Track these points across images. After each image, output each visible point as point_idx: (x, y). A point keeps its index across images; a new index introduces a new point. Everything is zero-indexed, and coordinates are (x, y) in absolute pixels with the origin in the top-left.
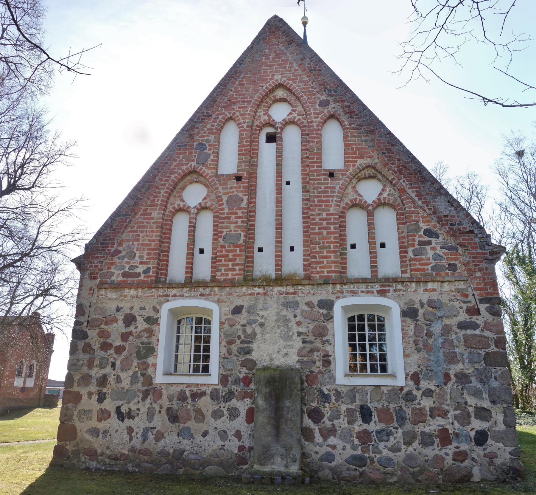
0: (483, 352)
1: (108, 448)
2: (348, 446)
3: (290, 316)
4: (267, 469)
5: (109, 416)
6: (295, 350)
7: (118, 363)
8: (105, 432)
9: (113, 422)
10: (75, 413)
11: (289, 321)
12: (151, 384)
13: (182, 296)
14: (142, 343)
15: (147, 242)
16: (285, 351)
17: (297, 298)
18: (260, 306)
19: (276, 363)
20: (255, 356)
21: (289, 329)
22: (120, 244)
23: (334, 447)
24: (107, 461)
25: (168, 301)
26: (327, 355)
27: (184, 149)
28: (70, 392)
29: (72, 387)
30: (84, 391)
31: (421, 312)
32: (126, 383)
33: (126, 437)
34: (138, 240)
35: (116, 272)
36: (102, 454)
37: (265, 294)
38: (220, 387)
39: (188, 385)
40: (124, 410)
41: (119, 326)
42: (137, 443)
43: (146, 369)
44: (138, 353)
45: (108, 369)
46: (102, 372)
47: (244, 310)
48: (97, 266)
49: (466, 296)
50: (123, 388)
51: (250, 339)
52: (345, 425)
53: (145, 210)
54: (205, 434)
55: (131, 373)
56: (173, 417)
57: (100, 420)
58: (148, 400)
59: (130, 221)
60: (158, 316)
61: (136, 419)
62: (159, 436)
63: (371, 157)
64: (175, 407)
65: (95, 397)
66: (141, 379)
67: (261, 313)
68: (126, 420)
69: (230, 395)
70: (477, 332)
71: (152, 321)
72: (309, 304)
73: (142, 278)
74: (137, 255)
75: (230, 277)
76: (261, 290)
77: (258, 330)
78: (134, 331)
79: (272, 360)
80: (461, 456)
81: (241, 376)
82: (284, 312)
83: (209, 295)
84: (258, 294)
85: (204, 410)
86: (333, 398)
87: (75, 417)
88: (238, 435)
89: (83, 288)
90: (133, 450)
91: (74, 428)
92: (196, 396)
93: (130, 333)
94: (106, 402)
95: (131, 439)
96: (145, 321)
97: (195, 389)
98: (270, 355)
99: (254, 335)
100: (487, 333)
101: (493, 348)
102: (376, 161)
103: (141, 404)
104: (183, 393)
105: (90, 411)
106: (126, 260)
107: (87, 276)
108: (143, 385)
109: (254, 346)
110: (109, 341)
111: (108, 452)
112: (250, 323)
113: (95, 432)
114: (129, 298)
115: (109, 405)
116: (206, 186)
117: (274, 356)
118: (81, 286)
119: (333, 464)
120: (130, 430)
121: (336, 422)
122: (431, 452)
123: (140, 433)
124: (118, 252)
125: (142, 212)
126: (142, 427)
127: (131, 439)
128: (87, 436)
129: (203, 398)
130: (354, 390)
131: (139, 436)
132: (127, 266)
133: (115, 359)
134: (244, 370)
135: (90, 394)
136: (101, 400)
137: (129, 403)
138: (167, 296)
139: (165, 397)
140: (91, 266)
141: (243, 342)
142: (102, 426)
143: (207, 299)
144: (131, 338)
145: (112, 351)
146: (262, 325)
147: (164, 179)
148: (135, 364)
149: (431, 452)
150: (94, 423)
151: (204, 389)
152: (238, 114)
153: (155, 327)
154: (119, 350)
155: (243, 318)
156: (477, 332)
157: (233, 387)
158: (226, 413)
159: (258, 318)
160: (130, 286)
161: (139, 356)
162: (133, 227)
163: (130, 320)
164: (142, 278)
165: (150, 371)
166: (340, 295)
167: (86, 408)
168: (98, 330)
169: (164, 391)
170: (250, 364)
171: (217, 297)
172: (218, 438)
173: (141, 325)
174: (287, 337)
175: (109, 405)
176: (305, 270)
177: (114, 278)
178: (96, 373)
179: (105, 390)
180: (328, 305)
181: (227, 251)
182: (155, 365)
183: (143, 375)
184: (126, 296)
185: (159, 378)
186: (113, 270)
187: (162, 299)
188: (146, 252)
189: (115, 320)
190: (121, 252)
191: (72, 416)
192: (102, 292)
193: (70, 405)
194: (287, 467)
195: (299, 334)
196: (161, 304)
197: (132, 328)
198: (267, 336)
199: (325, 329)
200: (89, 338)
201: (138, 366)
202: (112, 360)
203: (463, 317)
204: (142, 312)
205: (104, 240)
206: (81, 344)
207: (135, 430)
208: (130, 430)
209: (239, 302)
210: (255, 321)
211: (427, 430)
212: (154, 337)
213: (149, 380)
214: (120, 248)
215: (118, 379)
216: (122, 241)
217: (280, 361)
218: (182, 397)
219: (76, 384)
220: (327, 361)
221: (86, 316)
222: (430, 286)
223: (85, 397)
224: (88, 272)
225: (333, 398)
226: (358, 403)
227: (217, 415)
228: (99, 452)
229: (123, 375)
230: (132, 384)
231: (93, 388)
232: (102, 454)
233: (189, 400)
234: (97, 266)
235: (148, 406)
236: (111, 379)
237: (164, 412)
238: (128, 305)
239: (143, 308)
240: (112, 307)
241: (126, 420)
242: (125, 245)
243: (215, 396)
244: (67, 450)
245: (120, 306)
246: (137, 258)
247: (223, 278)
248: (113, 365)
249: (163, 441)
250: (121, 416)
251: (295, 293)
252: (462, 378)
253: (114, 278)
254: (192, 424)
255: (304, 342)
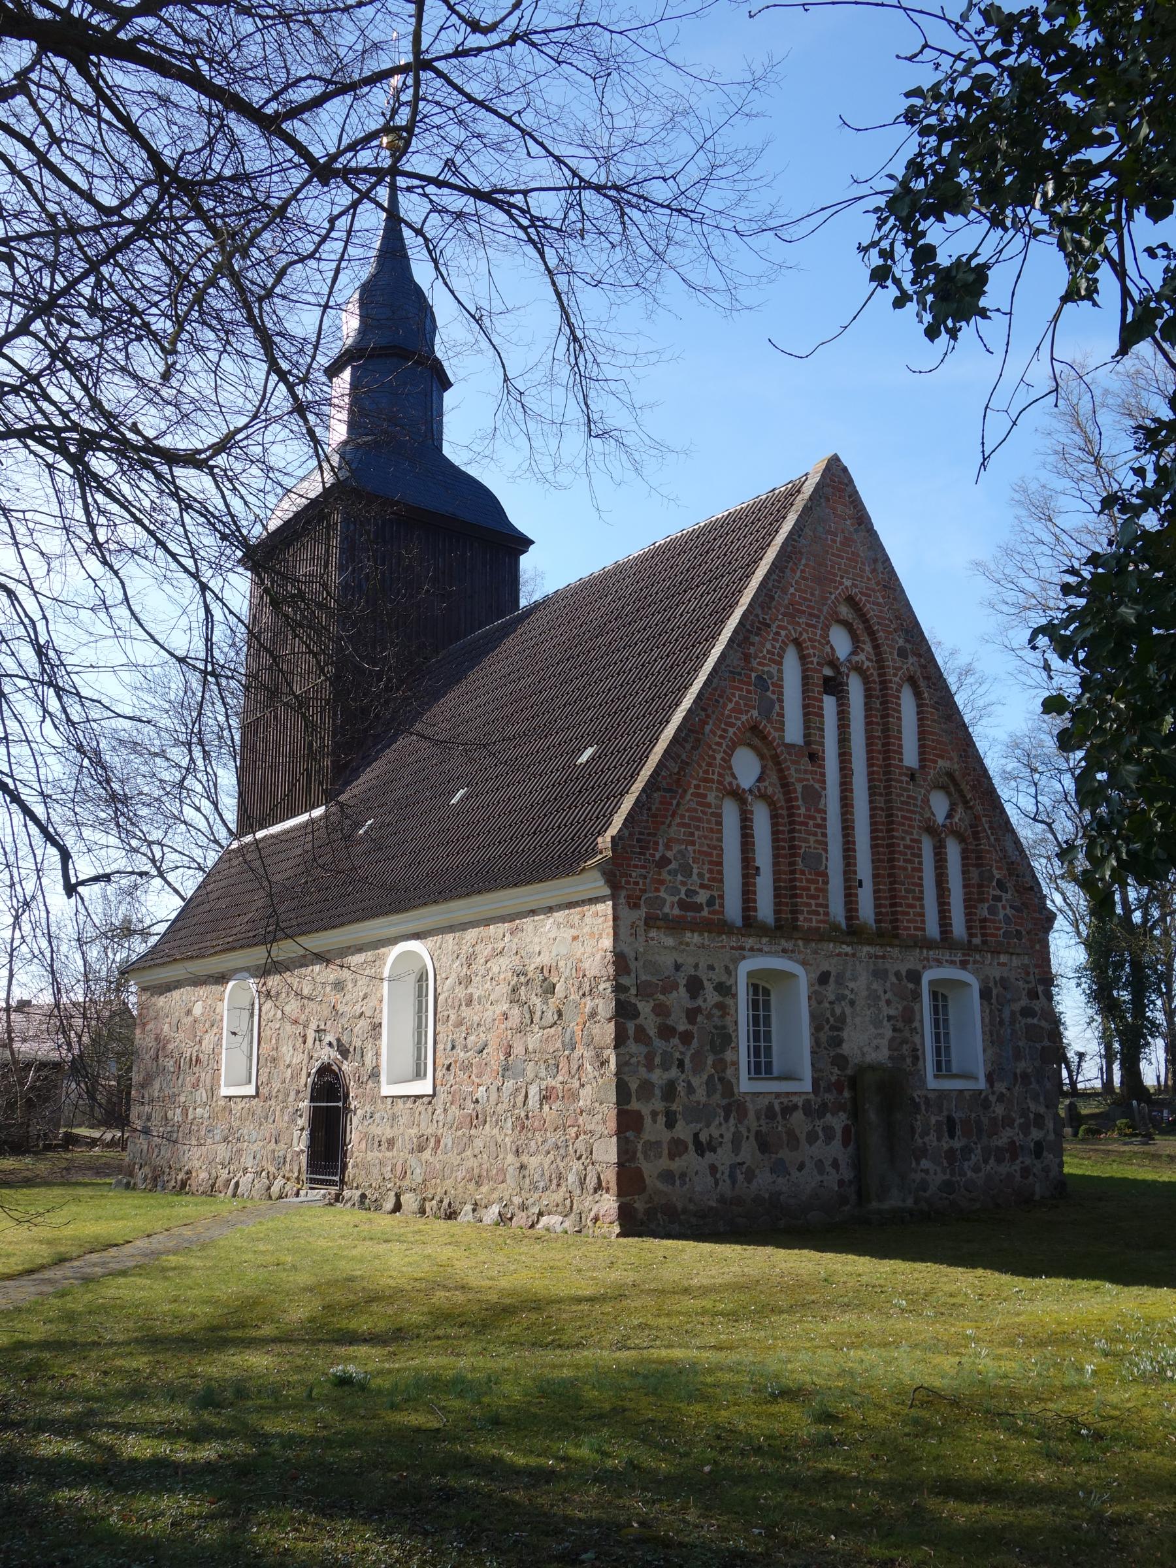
0: (1038, 1046)
1: (691, 1200)
2: (939, 1169)
3: (881, 992)
4: (886, 1206)
5: (686, 1148)
6: (885, 1042)
7: (687, 1061)
8: (683, 1175)
9: (690, 1160)
10: (640, 1147)
11: (879, 997)
12: (733, 1094)
13: (760, 950)
14: (716, 1027)
15: (705, 849)
16: (875, 1042)
17: (888, 966)
18: (848, 974)
19: (868, 1059)
20: (846, 1049)
21: (879, 1009)
22: (668, 847)
23: (927, 1172)
24: (694, 1220)
25: (744, 958)
26: (915, 1050)
27: (740, 681)
28: (627, 1111)
29: (629, 1102)
30: (646, 1111)
31: (995, 992)
32: (700, 1095)
33: (710, 1180)
34: (693, 843)
35: (670, 899)
36: (685, 1211)
37: (854, 955)
38: (812, 1096)
39: (778, 1095)
40: (703, 1138)
41: (679, 999)
42: (725, 1187)
43: (724, 1071)
44: (712, 1042)
45: (674, 1072)
46: (667, 1076)
47: (832, 979)
48: (636, 883)
49: (1028, 974)
50: (698, 1103)
51: (840, 1023)
52: (935, 1143)
53: (697, 787)
54: (801, 1167)
55: (705, 1077)
56: (764, 1145)
57: (672, 1157)
58: (732, 1121)
59: (678, 804)
60: (732, 981)
61: (719, 1150)
62: (750, 1176)
63: (951, 759)
64: (764, 1129)
65: (661, 1119)
66: (719, 1087)
67: (851, 985)
68: (707, 1154)
69: (823, 1110)
70: (1035, 1021)
71: (725, 990)
72: (897, 974)
73: (705, 913)
74: (695, 871)
75: (814, 924)
76: (848, 949)
77: (848, 1011)
78: (703, 1005)
79: (863, 1054)
80: (1026, 1171)
81: (834, 1079)
82: (875, 986)
83: (793, 951)
84: (846, 954)
85: (797, 1132)
86: (923, 1108)
87: (639, 1155)
88: (835, 1164)
89: (620, 923)
90: (722, 1200)
91: (639, 1171)
92: (788, 1110)
93: (698, 1010)
94: (680, 1125)
95: (717, 1184)
96: (715, 989)
97: (785, 1100)
98: (860, 1049)
99: (842, 1019)
100: (1044, 1024)
101: (1046, 1043)
102: (956, 766)
103: (724, 1126)
104: (770, 1107)
105: (658, 1144)
106: (680, 878)
107: (622, 900)
108: (723, 1096)
109: (845, 1035)
110: (670, 1022)
111: (691, 1207)
112: (841, 998)
113: (667, 1176)
114: (692, 948)
115: (683, 1131)
116: (762, 757)
117: (865, 1050)
118: (615, 919)
119: (927, 1195)
120: (713, 1169)
121: (926, 1139)
122: (1004, 1169)
123: (727, 1173)
124: (664, 862)
125: (692, 791)
126: (728, 1163)
127: (717, 1184)
128: (660, 1186)
129: (795, 1114)
130: (943, 1094)
131: (726, 1177)
132: (683, 890)
133: (682, 1053)
134: (836, 1070)
135: (654, 1114)
136: (670, 1124)
137: (708, 1126)
138: (742, 948)
139: (751, 1115)
140: (628, 883)
141: (832, 1028)
142: (676, 1165)
143: (790, 958)
144: (699, 1018)
145: (676, 1041)
146: (852, 1003)
147: (719, 733)
148: (710, 1062)
149: (1004, 1169)
150: (664, 1163)
151: (795, 1099)
152: (805, 636)
153: (729, 1001)
154: (686, 1038)
155: (830, 991)
156: (1035, 1021)
157: (827, 1095)
158: (821, 1134)
159: (847, 992)
160: (695, 927)
161: (714, 1050)
162: (682, 817)
163: (695, 986)
164: (705, 913)
165: (729, 1072)
166: (927, 964)
167: (653, 1139)
168: (652, 1004)
169: (750, 1106)
170: (840, 1061)
171: (802, 957)
172: (815, 1172)
173: (711, 997)
174: (877, 1023)
175: (683, 1131)
176: (877, 921)
177: (667, 910)
178: (658, 1077)
179: (674, 1107)
180: (915, 977)
181: (808, 881)
182: (735, 1064)
183: (721, 1079)
184: (688, 944)
185: (745, 1085)
186: (662, 894)
187: (736, 953)
188: (706, 867)
189: (675, 986)
190: (670, 862)
191: (635, 1153)
192: (653, 933)
193: (630, 1134)
194: (904, 1201)
195: (890, 1018)
196: (736, 961)
197: (700, 1002)
198: (858, 1020)
199: (912, 1011)
200: (642, 1016)
201: (714, 1066)
202: (677, 1055)
203: (1024, 1002)
204: (711, 974)
205: (641, 833)
206: (631, 1027)
207: (721, 1168)
208: (713, 1169)
209: (825, 967)
210: (844, 997)
211: (1000, 1143)
212: (728, 1018)
213: (728, 1088)
214: (669, 854)
215: (690, 1089)
216: (670, 840)
217: (872, 1057)
218: (770, 1113)
219: (634, 1099)
220: (916, 1056)
221: (633, 975)
222: (1003, 958)
223: (648, 1120)
224: (623, 893)
225: (923, 1108)
226: (945, 1113)
227: (812, 1138)
228: (679, 1206)
229: (696, 1082)
230: (708, 1096)
231: (658, 1105)
232: (685, 1211)
233: (779, 1118)
234: (636, 883)
235: (732, 1129)
236: (681, 1088)
237: (752, 1138)
238: (691, 961)
239: (711, 968)
240: (667, 960)
241: (707, 1154)
242: (676, 848)
243: (807, 1109)
244: (635, 1209)
245: (680, 961)
246: (695, 877)
247: (806, 925)
248: (681, 1065)
249: (755, 1182)
250: (700, 1149)
251: (883, 957)
252: (1025, 1076)
253: (667, 910)
254: (784, 1154)
255: (894, 1030)
